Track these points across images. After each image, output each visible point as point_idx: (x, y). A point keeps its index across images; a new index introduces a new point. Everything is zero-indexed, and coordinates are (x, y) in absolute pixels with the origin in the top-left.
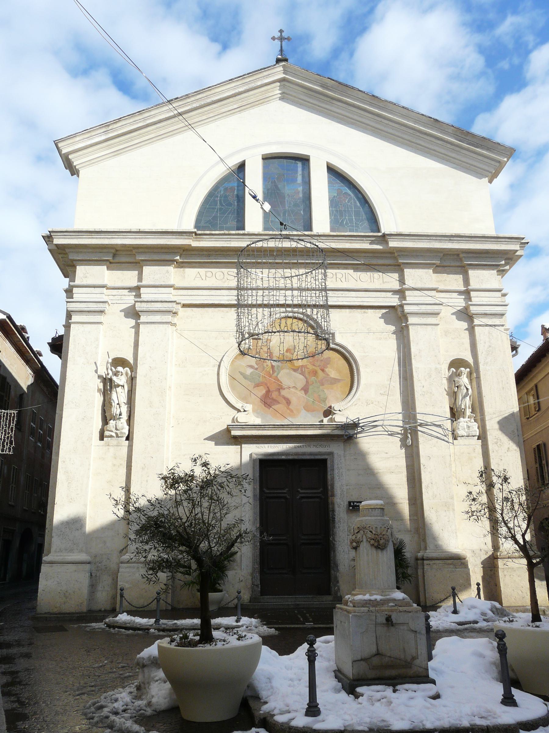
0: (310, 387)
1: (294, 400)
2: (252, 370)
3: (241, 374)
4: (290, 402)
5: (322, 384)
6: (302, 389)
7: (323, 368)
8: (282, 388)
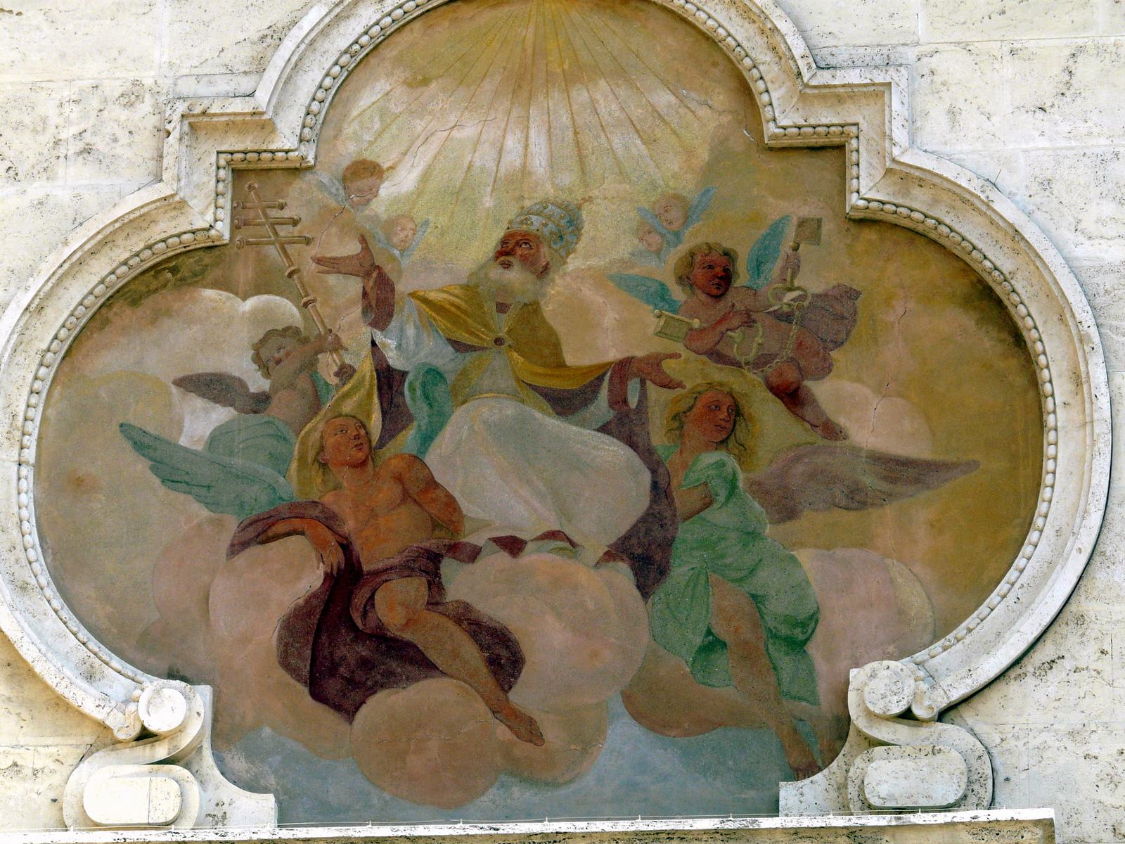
0: (686, 533)
1: (546, 640)
2: (221, 415)
3: (142, 442)
4: (517, 662)
5: (786, 511)
6: (620, 550)
7: (791, 375)
8: (454, 549)
